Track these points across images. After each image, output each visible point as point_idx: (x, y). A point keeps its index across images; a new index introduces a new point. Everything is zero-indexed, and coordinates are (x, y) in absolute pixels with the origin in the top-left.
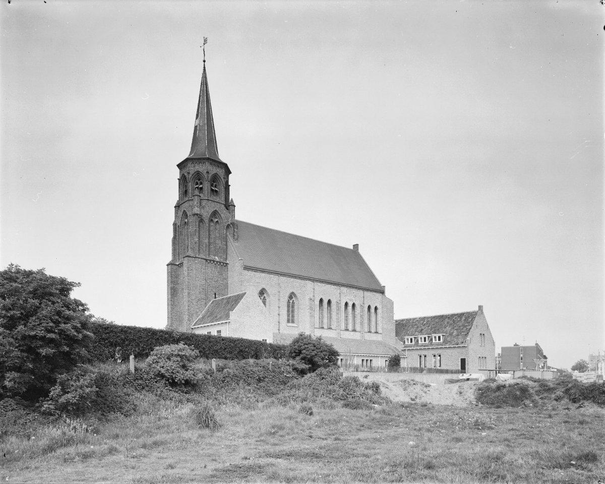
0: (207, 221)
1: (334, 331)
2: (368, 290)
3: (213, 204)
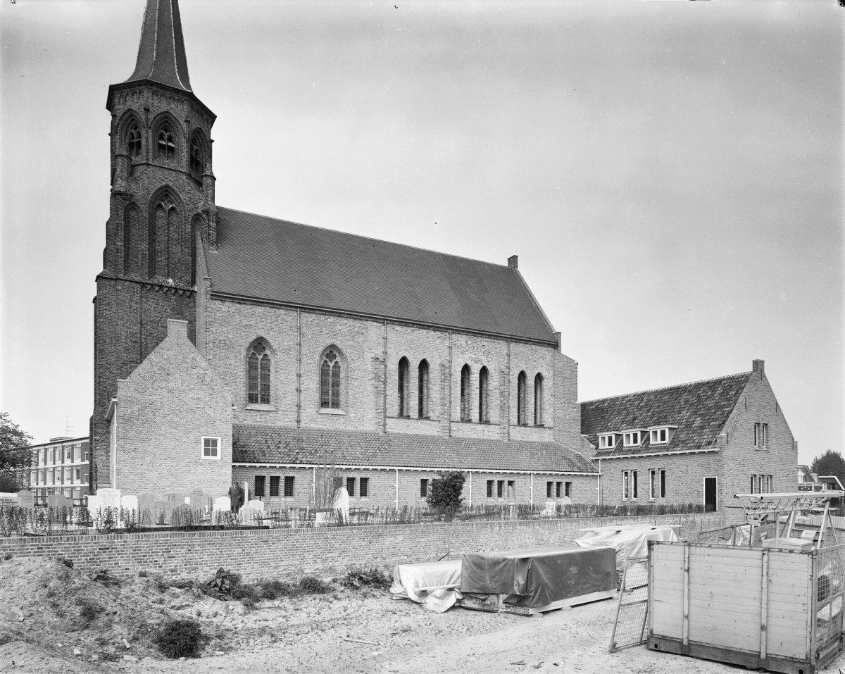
0: (144, 207)
1: (548, 431)
2: (518, 340)
3: (160, 173)
